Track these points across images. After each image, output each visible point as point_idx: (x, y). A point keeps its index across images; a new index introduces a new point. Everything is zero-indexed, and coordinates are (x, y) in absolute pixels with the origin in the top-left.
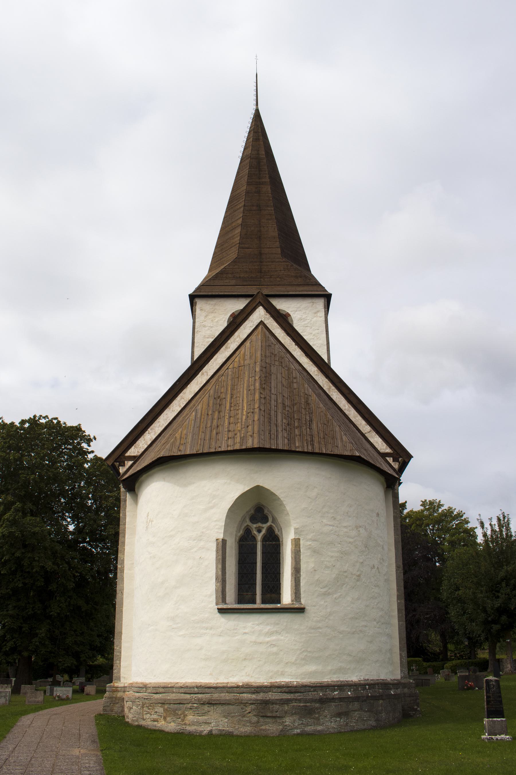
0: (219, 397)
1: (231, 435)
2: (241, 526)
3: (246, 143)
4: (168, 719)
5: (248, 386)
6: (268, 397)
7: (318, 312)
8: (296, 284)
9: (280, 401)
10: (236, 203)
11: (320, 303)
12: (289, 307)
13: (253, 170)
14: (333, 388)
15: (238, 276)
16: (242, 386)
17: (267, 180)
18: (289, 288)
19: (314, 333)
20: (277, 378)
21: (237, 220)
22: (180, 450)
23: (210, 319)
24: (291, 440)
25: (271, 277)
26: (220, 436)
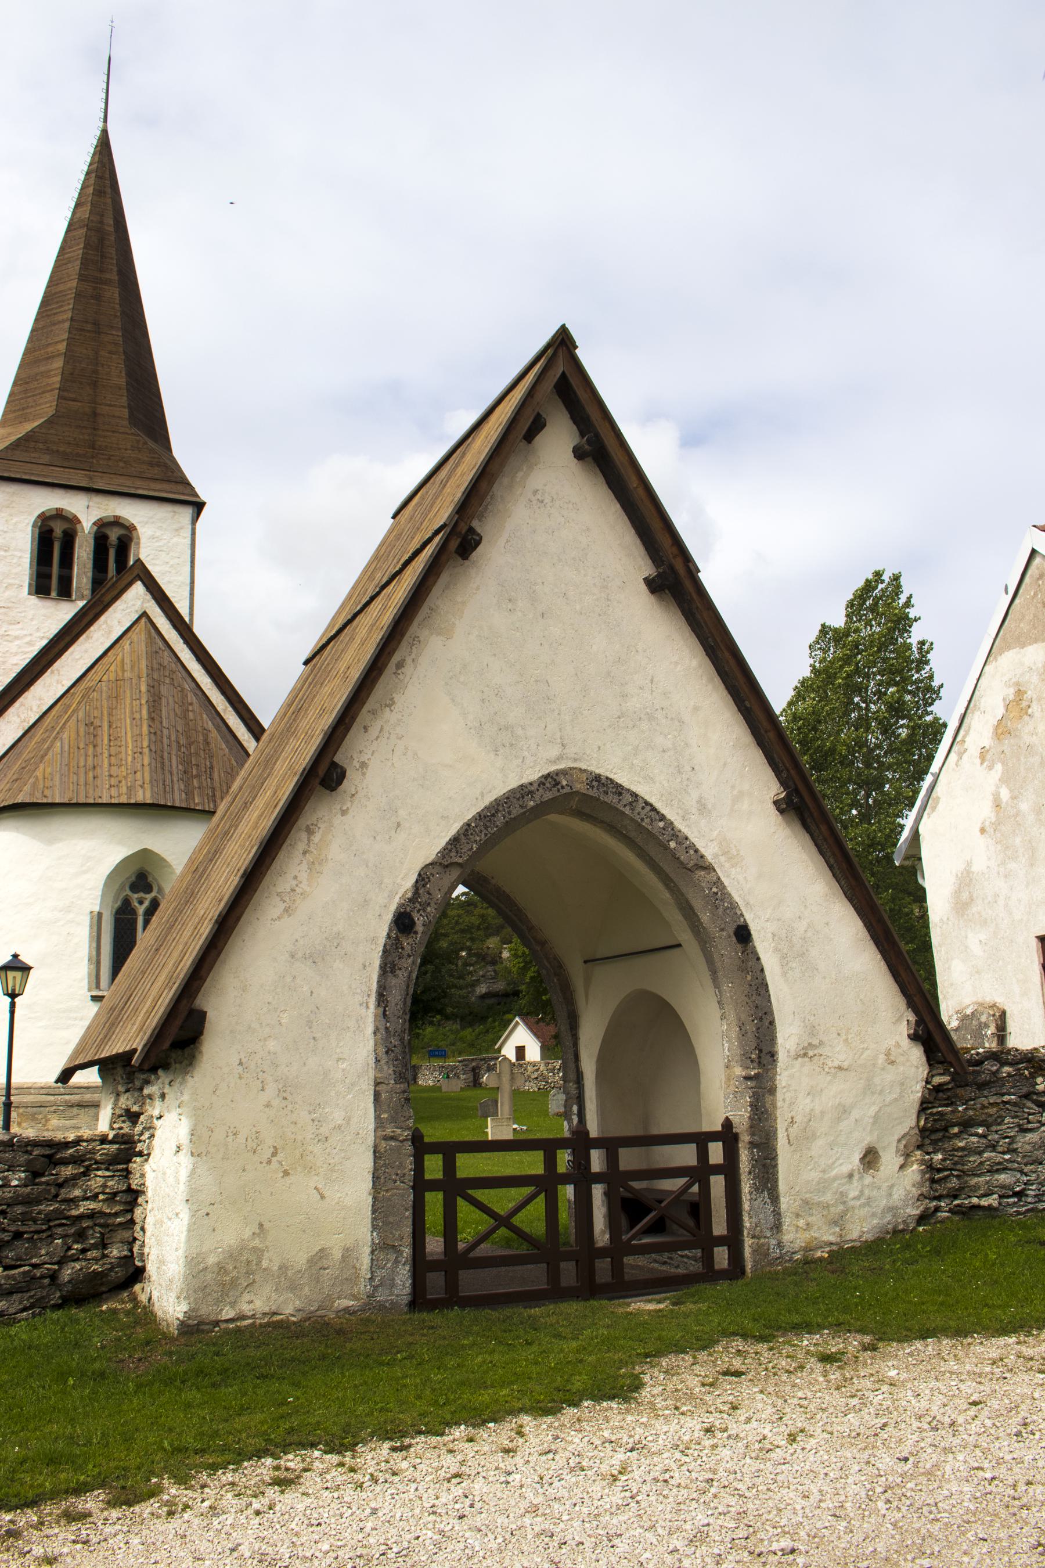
0: (92, 723)
1: (113, 781)
2: (118, 898)
3: (80, 194)
4: (24, 1125)
5: (132, 713)
6: (159, 732)
8: (150, 476)
9: (173, 738)
10: (56, 308)
12: (135, 515)
13: (90, 252)
14: (230, 709)
15: (55, 448)
16: (123, 711)
17: (114, 276)
18: (138, 483)
20: (168, 703)
21: (57, 342)
22: (45, 797)
24: (190, 794)
25: (110, 459)
26: (99, 782)
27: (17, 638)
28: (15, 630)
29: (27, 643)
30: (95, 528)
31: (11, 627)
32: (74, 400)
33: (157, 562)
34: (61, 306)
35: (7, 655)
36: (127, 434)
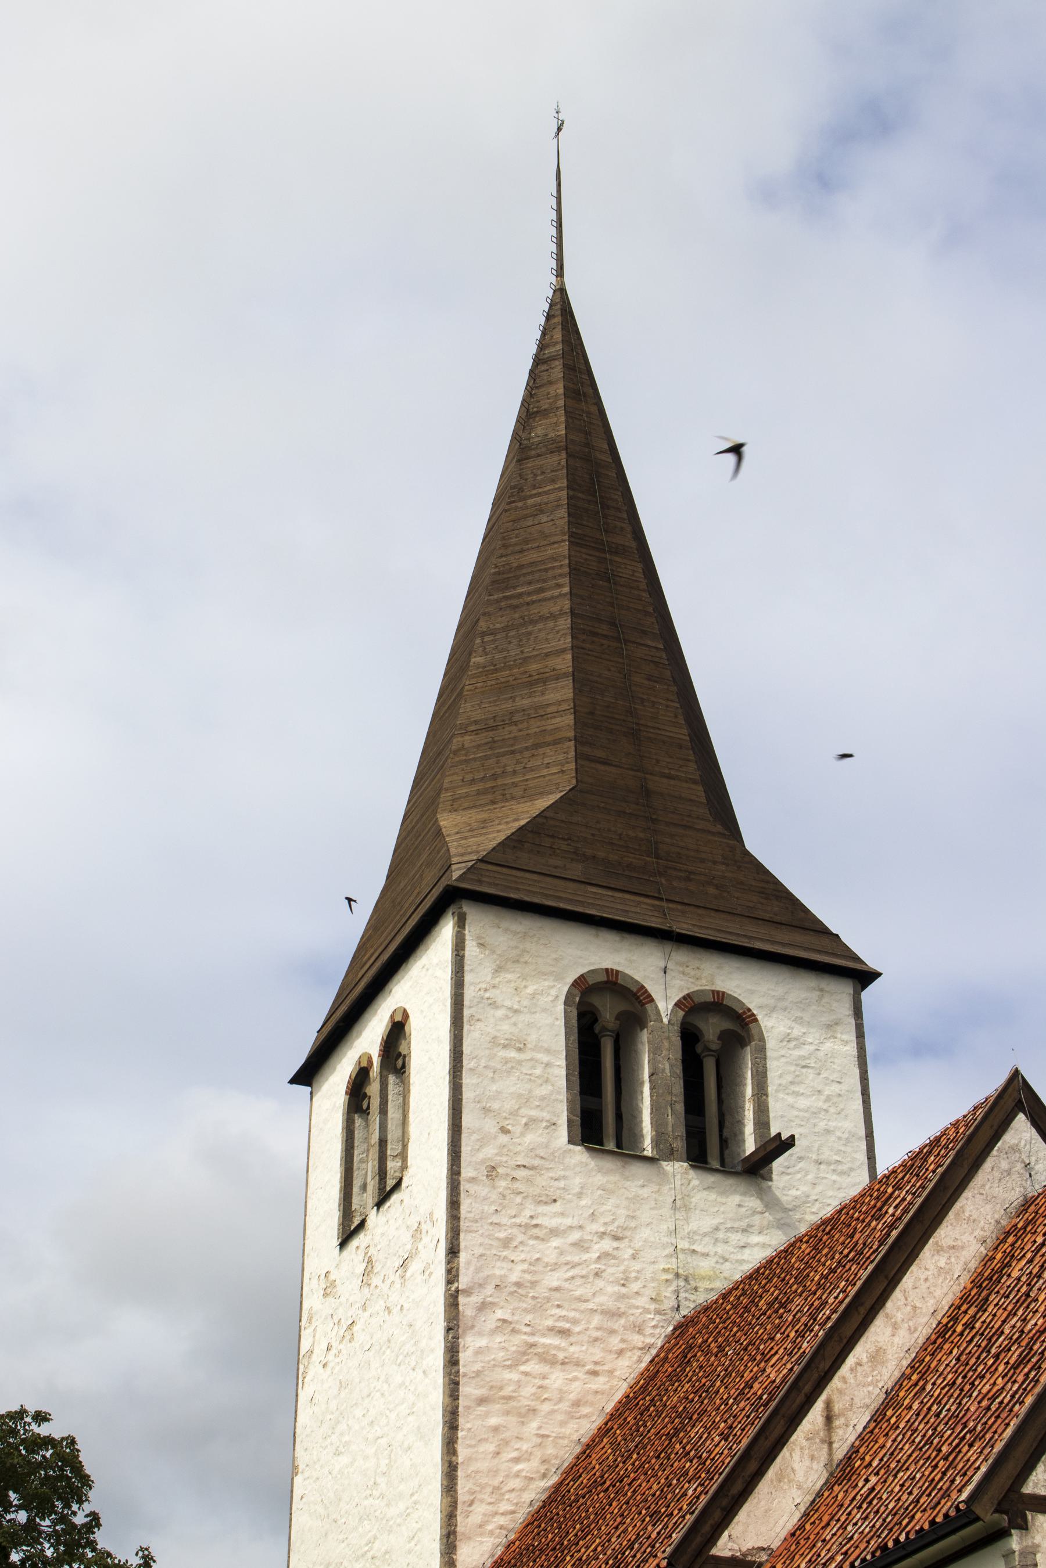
7: (836, 1024)
8: (767, 916)
10: (529, 594)
11: (841, 991)
12: (752, 992)
19: (826, 1093)
23: (509, 982)
27: (554, 1232)
28: (549, 1217)
29: (574, 1244)
30: (681, 1013)
31: (542, 1209)
32: (605, 763)
33: (800, 1089)
34: (542, 590)
35: (539, 1268)
36: (709, 832)
